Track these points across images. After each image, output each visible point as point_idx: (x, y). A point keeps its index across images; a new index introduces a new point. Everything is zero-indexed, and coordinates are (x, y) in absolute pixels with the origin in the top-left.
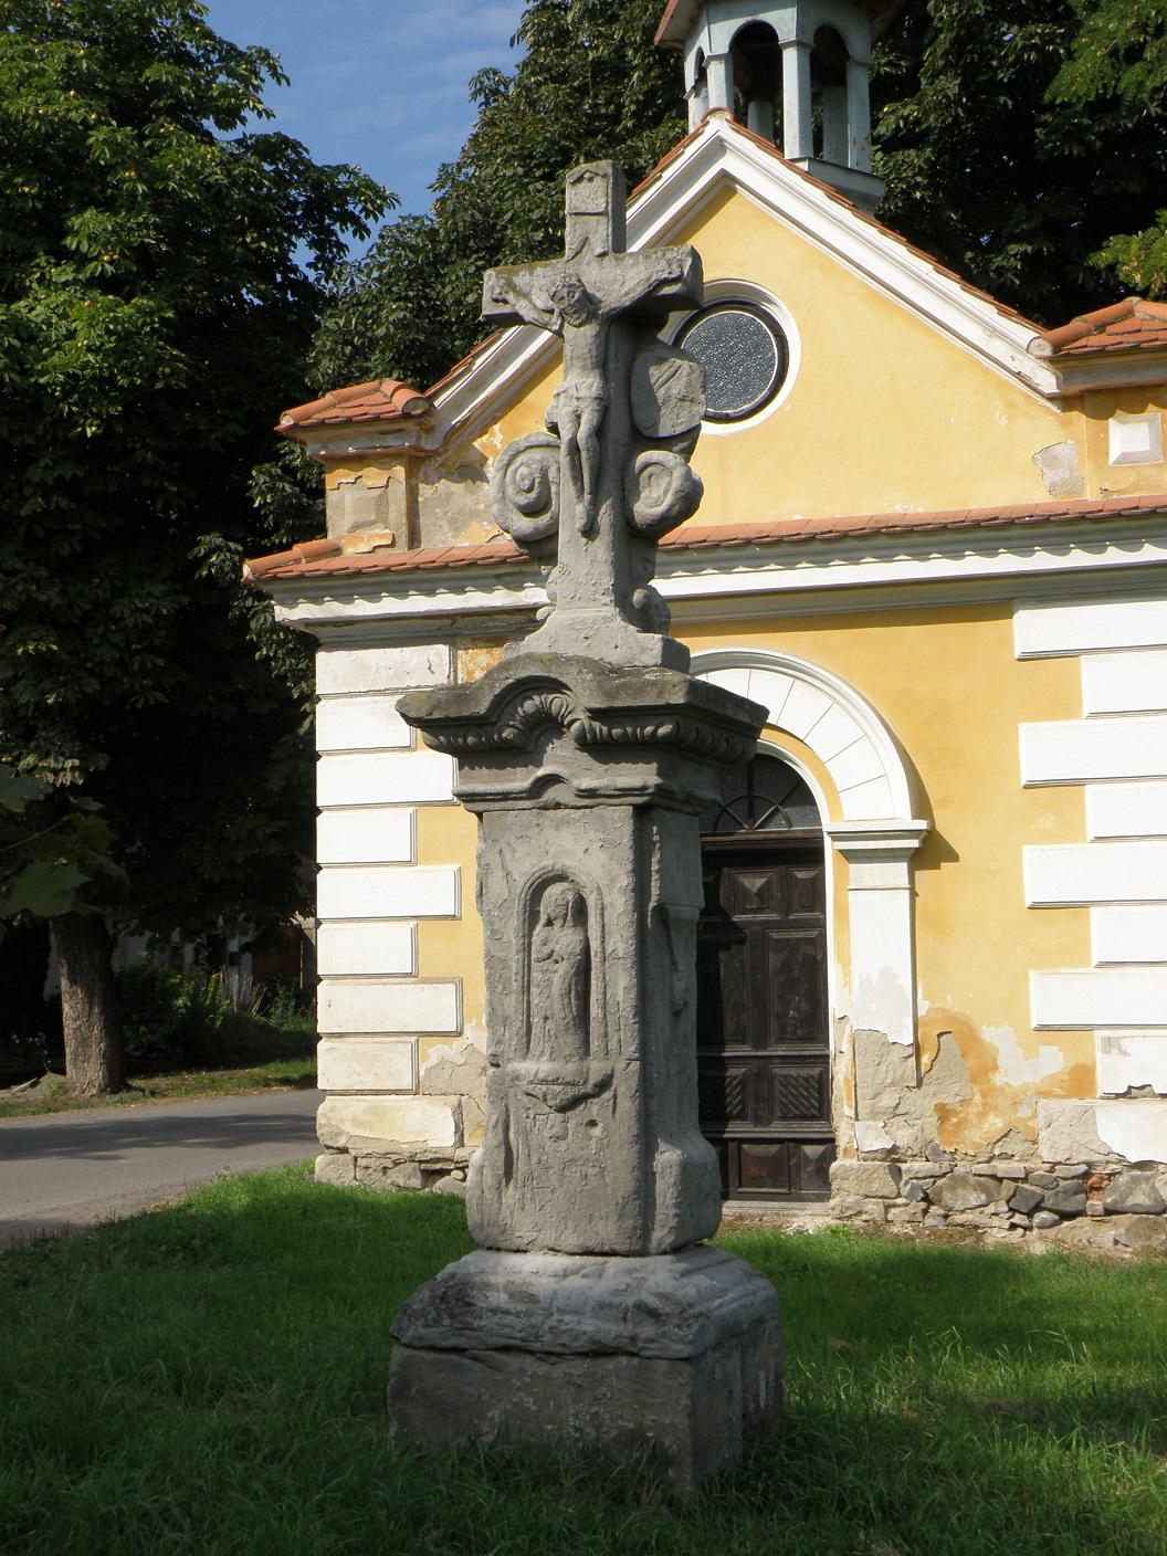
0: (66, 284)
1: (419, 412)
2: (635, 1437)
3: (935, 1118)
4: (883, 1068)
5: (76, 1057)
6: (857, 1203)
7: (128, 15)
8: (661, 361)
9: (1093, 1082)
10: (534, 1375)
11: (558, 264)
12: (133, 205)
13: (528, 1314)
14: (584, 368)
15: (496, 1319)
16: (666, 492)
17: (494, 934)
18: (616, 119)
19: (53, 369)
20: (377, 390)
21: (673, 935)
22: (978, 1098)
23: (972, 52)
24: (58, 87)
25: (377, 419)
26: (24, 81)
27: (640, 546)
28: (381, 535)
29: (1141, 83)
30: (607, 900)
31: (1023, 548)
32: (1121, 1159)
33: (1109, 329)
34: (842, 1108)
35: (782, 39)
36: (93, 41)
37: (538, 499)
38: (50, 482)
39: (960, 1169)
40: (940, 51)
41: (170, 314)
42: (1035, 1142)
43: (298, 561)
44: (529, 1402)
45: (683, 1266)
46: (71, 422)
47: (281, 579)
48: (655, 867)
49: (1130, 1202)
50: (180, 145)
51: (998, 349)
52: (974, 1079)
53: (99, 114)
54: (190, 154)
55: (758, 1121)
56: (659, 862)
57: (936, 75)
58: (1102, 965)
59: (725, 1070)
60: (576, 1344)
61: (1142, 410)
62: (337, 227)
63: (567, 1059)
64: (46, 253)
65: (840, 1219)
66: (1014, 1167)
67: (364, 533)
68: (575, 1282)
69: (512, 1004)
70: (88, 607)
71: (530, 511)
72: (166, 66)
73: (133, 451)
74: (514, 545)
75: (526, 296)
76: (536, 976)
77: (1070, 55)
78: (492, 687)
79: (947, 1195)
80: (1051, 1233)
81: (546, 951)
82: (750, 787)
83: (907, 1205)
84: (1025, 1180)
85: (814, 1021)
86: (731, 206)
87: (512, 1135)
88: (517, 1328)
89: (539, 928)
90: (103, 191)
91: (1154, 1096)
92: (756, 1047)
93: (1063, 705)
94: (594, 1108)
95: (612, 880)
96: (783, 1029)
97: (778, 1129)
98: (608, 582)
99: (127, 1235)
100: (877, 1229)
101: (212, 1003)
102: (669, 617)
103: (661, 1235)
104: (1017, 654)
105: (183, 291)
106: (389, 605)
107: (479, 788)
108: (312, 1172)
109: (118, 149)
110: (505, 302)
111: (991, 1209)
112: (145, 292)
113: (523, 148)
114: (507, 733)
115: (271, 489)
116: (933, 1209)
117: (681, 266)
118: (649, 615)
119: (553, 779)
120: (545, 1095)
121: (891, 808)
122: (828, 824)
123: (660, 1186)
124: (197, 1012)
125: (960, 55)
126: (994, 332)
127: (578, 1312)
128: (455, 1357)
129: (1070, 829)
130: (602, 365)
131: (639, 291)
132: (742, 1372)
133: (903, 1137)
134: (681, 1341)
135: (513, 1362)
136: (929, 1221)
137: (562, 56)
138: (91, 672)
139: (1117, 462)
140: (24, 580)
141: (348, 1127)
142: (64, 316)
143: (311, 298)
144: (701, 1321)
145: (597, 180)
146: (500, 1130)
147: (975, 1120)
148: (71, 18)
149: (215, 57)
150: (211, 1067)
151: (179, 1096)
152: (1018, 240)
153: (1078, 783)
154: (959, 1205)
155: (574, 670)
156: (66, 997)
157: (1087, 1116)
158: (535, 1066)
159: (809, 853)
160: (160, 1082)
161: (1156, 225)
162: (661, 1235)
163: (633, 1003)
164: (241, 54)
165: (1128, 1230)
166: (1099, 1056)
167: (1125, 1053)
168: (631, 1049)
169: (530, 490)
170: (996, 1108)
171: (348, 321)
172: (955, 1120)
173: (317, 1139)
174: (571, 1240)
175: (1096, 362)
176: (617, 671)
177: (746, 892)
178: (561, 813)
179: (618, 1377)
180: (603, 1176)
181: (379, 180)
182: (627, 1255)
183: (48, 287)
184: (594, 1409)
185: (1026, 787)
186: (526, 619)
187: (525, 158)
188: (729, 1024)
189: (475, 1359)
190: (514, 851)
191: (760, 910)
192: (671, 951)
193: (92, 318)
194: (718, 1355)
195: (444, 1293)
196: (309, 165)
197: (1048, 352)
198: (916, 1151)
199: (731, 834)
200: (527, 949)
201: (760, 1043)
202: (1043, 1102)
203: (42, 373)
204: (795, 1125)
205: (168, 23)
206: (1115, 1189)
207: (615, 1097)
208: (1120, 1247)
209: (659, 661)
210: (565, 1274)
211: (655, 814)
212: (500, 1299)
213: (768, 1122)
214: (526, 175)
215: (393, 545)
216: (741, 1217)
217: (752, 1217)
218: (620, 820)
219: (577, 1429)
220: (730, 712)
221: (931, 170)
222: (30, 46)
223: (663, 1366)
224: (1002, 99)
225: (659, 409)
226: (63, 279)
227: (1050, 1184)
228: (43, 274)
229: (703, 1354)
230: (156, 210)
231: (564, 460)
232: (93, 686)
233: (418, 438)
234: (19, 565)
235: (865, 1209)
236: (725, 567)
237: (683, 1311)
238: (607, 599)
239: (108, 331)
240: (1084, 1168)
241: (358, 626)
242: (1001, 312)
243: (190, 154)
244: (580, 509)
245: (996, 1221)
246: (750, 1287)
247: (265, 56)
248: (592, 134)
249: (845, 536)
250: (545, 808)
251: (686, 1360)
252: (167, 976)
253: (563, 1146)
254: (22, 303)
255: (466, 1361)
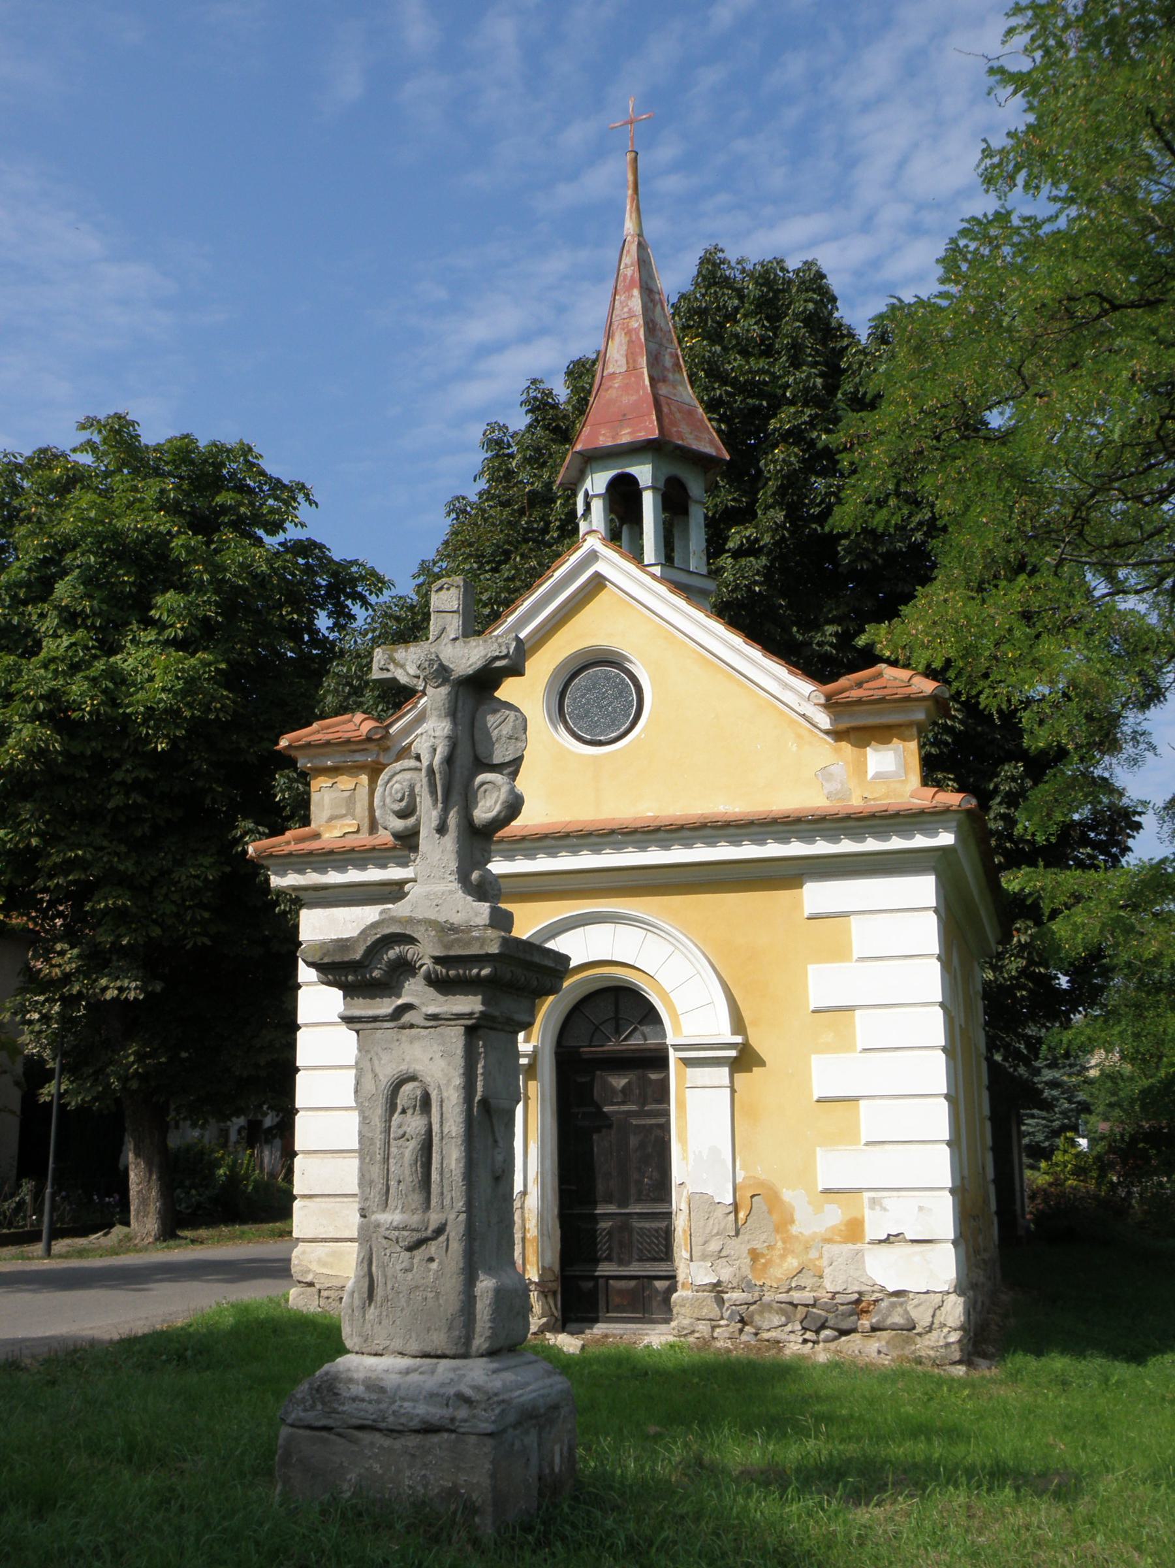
0: (150, 643)
1: (378, 736)
2: (452, 1493)
3: (748, 1260)
4: (711, 1221)
5: (138, 1213)
6: (691, 1324)
7: (206, 461)
8: (495, 711)
9: (863, 1231)
10: (381, 1447)
11: (425, 645)
12: (201, 588)
13: (378, 1402)
14: (439, 716)
15: (354, 1405)
16: (496, 802)
17: (365, 1120)
18: (545, 530)
19: (136, 703)
20: (350, 721)
21: (495, 1121)
22: (780, 1244)
23: (792, 495)
24: (153, 509)
25: (348, 742)
26: (130, 505)
27: (479, 839)
28: (349, 824)
29: (888, 521)
30: (445, 1094)
31: (808, 838)
32: (882, 1289)
33: (865, 686)
34: (681, 1252)
35: (642, 484)
36: (181, 478)
37: (407, 806)
38: (129, 781)
39: (767, 1298)
40: (769, 493)
41: (223, 666)
42: (821, 1277)
43: (288, 843)
44: (377, 1467)
45: (495, 1365)
46: (147, 740)
47: (276, 856)
48: (480, 1071)
49: (889, 1321)
50: (236, 547)
51: (788, 697)
52: (777, 1230)
53: (180, 528)
54: (242, 554)
55: (621, 1262)
56: (484, 1067)
57: (768, 507)
58: (868, 1144)
59: (597, 1223)
60: (411, 1424)
61: (889, 742)
62: (349, 602)
63: (414, 1212)
64: (138, 622)
65: (680, 1336)
66: (806, 1296)
67: (338, 823)
68: (414, 1377)
69: (376, 1171)
70: (155, 874)
71: (403, 815)
72: (231, 494)
73: (192, 761)
74: (391, 838)
75: (402, 666)
76: (393, 1150)
77: (840, 501)
78: (365, 940)
79: (757, 1318)
80: (832, 1346)
81: (401, 1132)
82: (617, 1011)
83: (727, 1326)
84: (814, 1306)
85: (661, 1187)
86: (603, 596)
87: (374, 1268)
88: (369, 1412)
89: (396, 1115)
90: (180, 579)
91: (906, 1241)
92: (619, 1206)
93: (839, 951)
94: (433, 1248)
95: (449, 1081)
96: (640, 1192)
97: (635, 1269)
98: (453, 865)
99: (137, 1347)
100: (705, 1343)
101: (246, 1173)
102: (500, 890)
103: (480, 1342)
104: (806, 915)
105: (233, 648)
106: (353, 876)
107: (357, 1013)
108: (287, 1301)
109: (190, 550)
110: (388, 670)
111: (789, 1328)
112: (205, 649)
113: (477, 550)
114: (376, 974)
115: (289, 788)
116: (747, 1328)
117: (508, 648)
118: (484, 889)
119: (408, 1007)
120: (397, 1239)
121: (719, 1028)
122: (670, 1040)
123: (479, 1306)
124: (234, 1179)
125: (783, 496)
126: (786, 686)
127: (414, 1400)
128: (324, 1434)
129: (845, 1043)
130: (452, 713)
131: (479, 664)
132: (539, 1445)
133: (726, 1274)
134: (486, 1420)
135: (366, 1437)
136: (744, 1338)
137: (507, 488)
138: (155, 922)
139: (874, 778)
140: (109, 854)
141: (314, 1267)
142: (147, 666)
143: (330, 651)
144: (503, 1406)
145: (453, 590)
146: (365, 1265)
147: (778, 1261)
148: (167, 463)
149: (266, 488)
150: (243, 1222)
151: (213, 1243)
152: (830, 622)
153: (850, 1009)
154: (766, 1326)
155: (422, 929)
156: (132, 1167)
157: (858, 1257)
158: (391, 1217)
159: (658, 1060)
160: (202, 1233)
161: (899, 616)
162: (480, 1342)
163: (462, 1170)
164: (285, 486)
165: (888, 1343)
166: (867, 1213)
167: (885, 1209)
168: (460, 1204)
169: (401, 800)
170: (793, 1251)
171: (349, 669)
172: (763, 1261)
173: (291, 1276)
174: (414, 1347)
175: (856, 708)
176: (454, 929)
177: (613, 1090)
178: (414, 1031)
179: (440, 1448)
180: (438, 1299)
181: (380, 570)
182: (454, 1357)
183: (137, 645)
184: (423, 1472)
185: (813, 1012)
186: (394, 891)
187: (479, 557)
188: (600, 1187)
189: (339, 1435)
190: (380, 1059)
191: (623, 1103)
192: (493, 1132)
193: (166, 667)
194: (518, 1432)
195: (320, 1386)
196: (331, 561)
197: (822, 701)
198: (735, 1285)
199: (602, 1046)
200: (388, 1130)
201: (623, 1203)
202: (827, 1246)
203: (128, 706)
204: (648, 1265)
205: (234, 466)
206: (880, 1311)
207: (448, 1240)
208: (882, 1355)
209: (487, 922)
210: (408, 1372)
211: (481, 1032)
212: (358, 1390)
213: (628, 1263)
214: (479, 569)
215: (358, 831)
216: (606, 1336)
217: (614, 1336)
218: (455, 1036)
219: (410, 1487)
220: (537, 959)
221: (768, 573)
222: (135, 482)
223: (473, 1439)
224: (814, 526)
225: (493, 745)
226: (148, 639)
227: (832, 1308)
228: (134, 637)
229: (504, 1431)
230: (217, 592)
231: (425, 780)
232: (156, 932)
233: (378, 755)
234: (105, 843)
235: (697, 1329)
236: (596, 849)
237: (489, 1399)
238: (453, 878)
239: (178, 678)
240: (856, 1296)
241: (336, 890)
242: (791, 672)
243: (242, 554)
244: (435, 814)
245: (792, 1337)
246: (548, 1381)
247: (302, 487)
248: (526, 541)
249: (682, 828)
250: (403, 1027)
251: (490, 1435)
252: (213, 1151)
253: (410, 1276)
254: (119, 657)
255: (333, 1437)
